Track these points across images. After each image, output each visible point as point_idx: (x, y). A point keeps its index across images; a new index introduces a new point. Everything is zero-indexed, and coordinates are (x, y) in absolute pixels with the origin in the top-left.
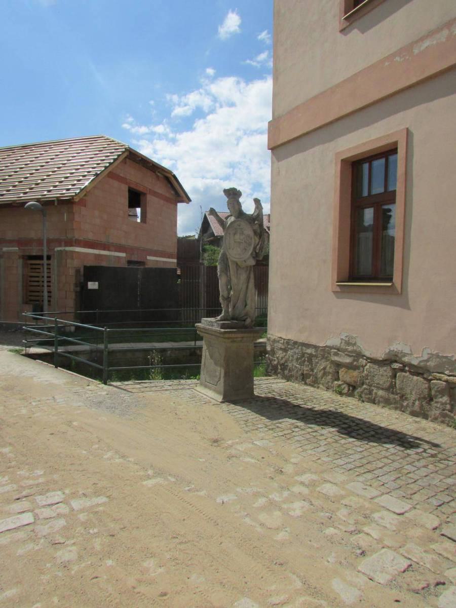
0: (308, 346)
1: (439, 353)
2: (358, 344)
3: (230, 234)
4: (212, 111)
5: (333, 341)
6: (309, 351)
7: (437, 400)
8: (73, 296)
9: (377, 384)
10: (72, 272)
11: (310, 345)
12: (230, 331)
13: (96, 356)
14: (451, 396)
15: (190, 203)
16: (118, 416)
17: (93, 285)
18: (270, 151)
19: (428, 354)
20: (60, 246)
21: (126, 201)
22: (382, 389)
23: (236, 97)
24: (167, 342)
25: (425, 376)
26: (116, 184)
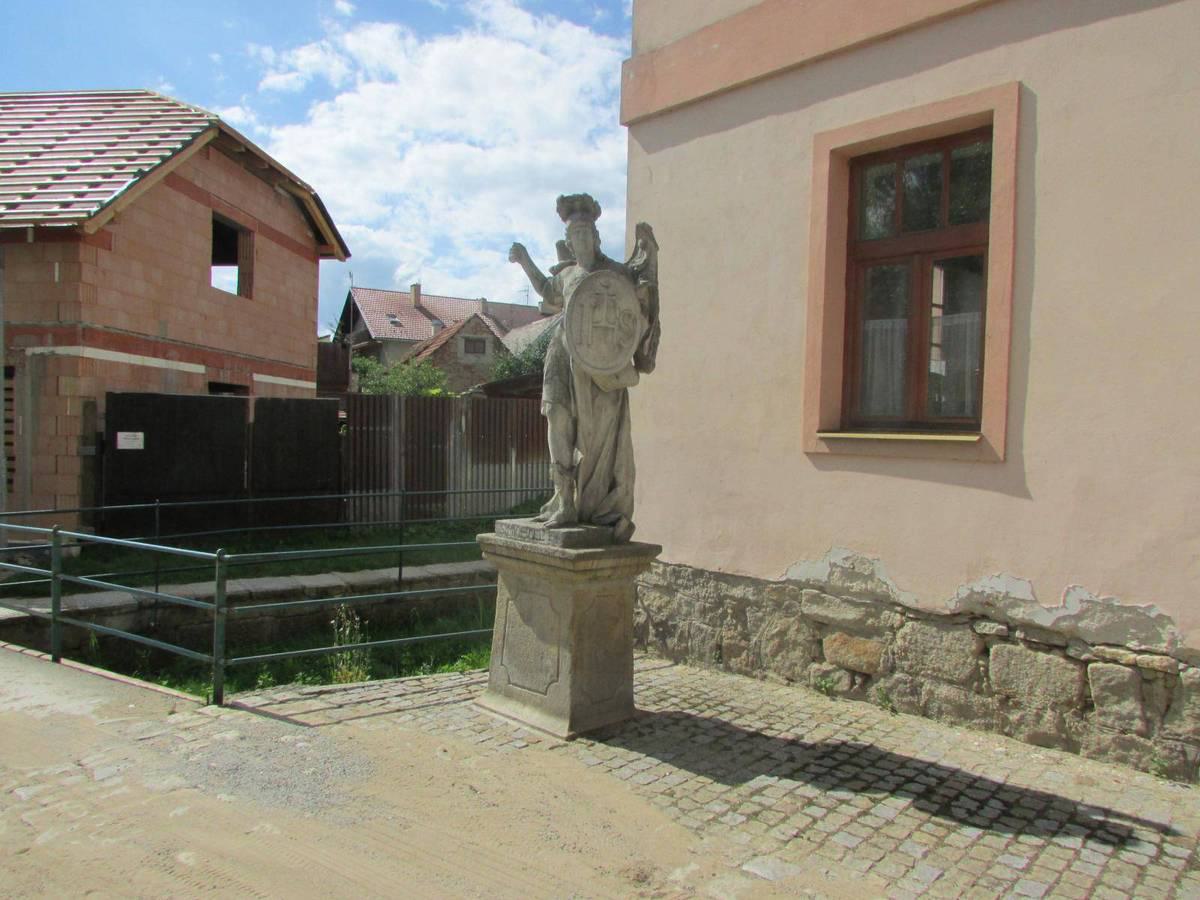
0: (734, 580)
1: (1113, 599)
2: (881, 575)
3: (582, 306)
4: (349, 87)
5: (812, 569)
7: (1105, 709)
8: (76, 466)
9: (934, 670)
10: (73, 409)
11: (742, 577)
12: (585, 554)
13: (148, 618)
14: (1144, 700)
15: (348, 260)
16: (308, 815)
17: (130, 441)
18: (627, 128)
19: (1082, 601)
20: (42, 344)
21: (206, 246)
22: (950, 682)
23: (398, 64)
24: (327, 572)
25: (1071, 652)
26: (183, 201)
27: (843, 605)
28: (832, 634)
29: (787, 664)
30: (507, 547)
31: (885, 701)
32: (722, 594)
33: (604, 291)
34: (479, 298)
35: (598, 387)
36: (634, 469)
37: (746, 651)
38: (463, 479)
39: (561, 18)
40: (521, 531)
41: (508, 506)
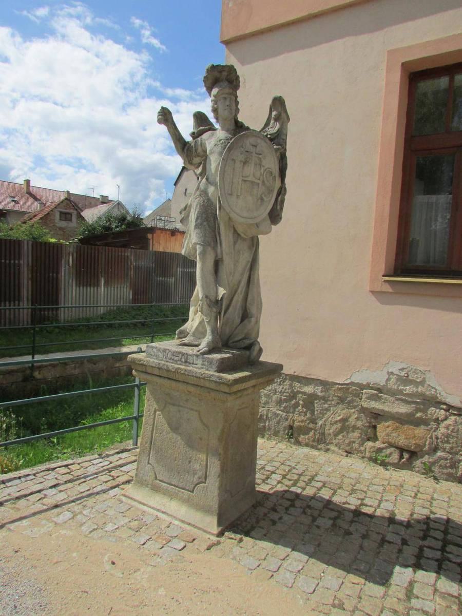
0: (307, 381)
6: (309, 389)
23: (11, 52)
27: (397, 402)
28: (386, 422)
29: (347, 441)
30: (159, 369)
31: (428, 471)
32: (295, 391)
33: (252, 149)
34: (65, 191)
35: (239, 235)
36: (261, 303)
37: (313, 431)
38: (70, 297)
39: (107, 38)
40: (173, 355)
41: (99, 313)
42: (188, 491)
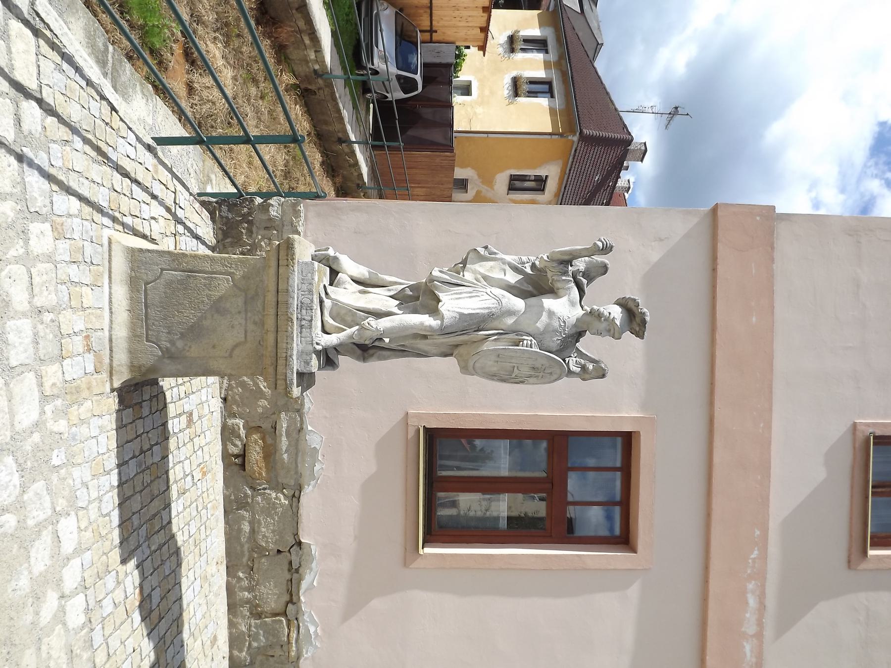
42: (147, 335)
